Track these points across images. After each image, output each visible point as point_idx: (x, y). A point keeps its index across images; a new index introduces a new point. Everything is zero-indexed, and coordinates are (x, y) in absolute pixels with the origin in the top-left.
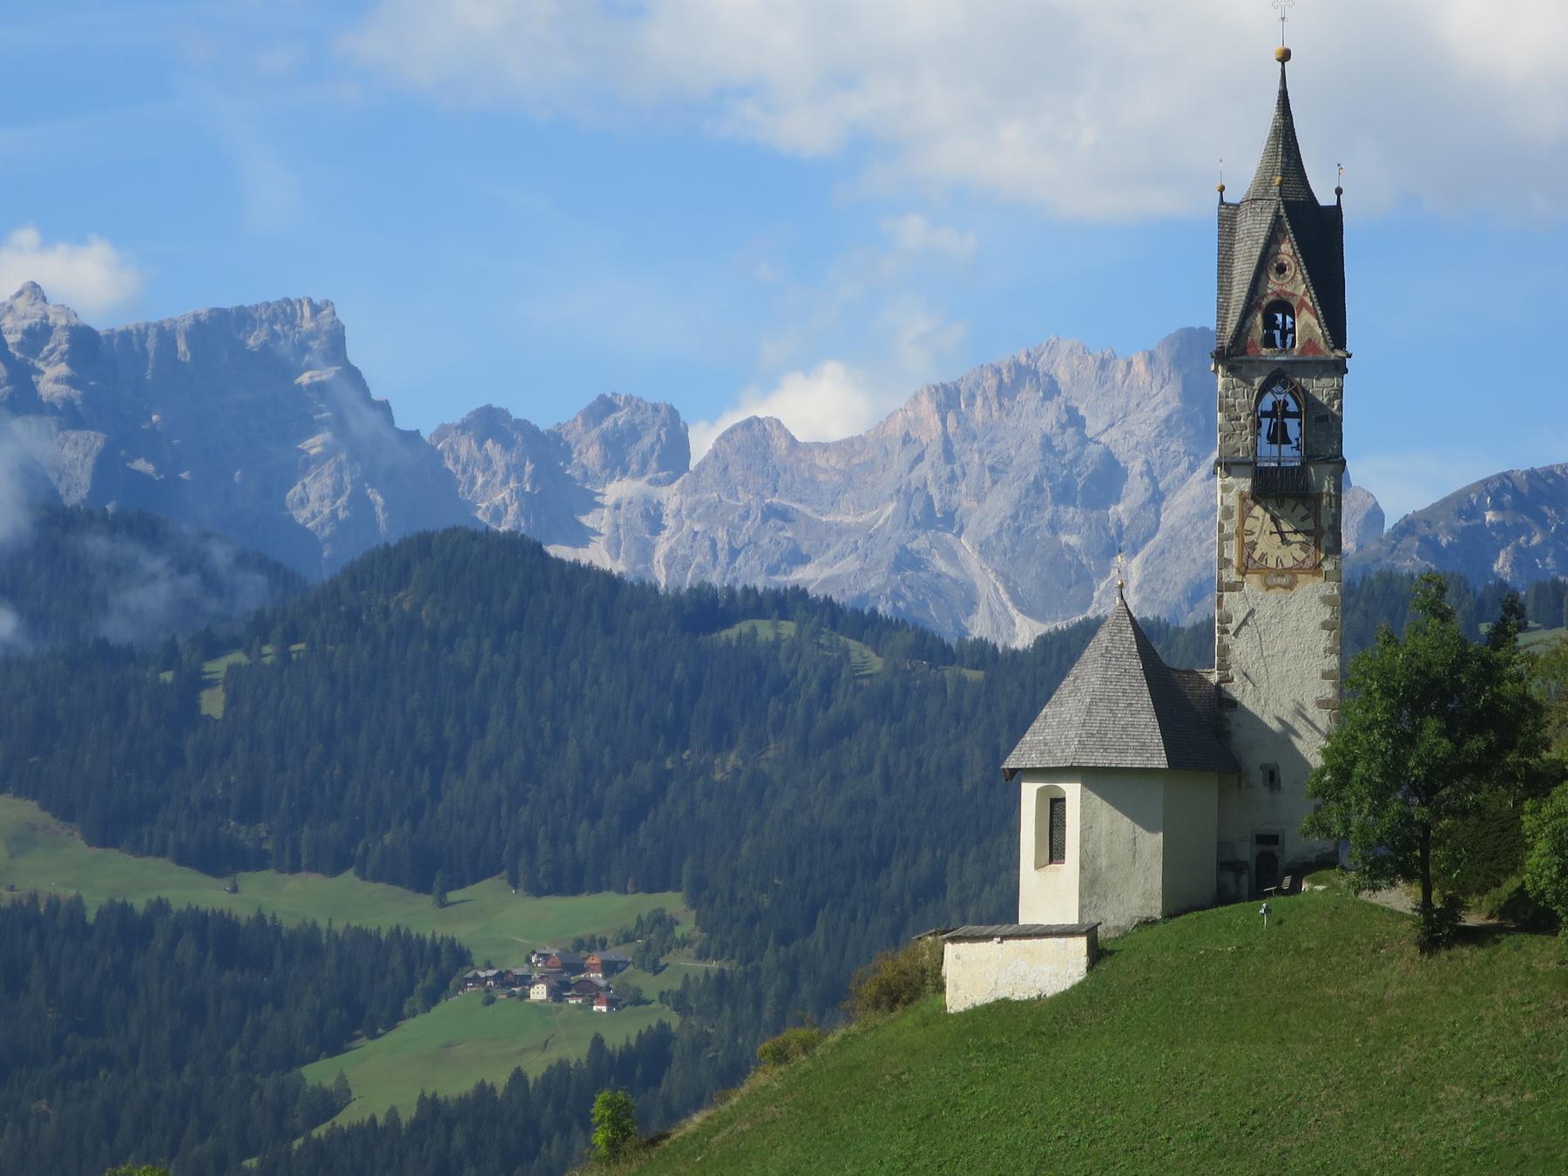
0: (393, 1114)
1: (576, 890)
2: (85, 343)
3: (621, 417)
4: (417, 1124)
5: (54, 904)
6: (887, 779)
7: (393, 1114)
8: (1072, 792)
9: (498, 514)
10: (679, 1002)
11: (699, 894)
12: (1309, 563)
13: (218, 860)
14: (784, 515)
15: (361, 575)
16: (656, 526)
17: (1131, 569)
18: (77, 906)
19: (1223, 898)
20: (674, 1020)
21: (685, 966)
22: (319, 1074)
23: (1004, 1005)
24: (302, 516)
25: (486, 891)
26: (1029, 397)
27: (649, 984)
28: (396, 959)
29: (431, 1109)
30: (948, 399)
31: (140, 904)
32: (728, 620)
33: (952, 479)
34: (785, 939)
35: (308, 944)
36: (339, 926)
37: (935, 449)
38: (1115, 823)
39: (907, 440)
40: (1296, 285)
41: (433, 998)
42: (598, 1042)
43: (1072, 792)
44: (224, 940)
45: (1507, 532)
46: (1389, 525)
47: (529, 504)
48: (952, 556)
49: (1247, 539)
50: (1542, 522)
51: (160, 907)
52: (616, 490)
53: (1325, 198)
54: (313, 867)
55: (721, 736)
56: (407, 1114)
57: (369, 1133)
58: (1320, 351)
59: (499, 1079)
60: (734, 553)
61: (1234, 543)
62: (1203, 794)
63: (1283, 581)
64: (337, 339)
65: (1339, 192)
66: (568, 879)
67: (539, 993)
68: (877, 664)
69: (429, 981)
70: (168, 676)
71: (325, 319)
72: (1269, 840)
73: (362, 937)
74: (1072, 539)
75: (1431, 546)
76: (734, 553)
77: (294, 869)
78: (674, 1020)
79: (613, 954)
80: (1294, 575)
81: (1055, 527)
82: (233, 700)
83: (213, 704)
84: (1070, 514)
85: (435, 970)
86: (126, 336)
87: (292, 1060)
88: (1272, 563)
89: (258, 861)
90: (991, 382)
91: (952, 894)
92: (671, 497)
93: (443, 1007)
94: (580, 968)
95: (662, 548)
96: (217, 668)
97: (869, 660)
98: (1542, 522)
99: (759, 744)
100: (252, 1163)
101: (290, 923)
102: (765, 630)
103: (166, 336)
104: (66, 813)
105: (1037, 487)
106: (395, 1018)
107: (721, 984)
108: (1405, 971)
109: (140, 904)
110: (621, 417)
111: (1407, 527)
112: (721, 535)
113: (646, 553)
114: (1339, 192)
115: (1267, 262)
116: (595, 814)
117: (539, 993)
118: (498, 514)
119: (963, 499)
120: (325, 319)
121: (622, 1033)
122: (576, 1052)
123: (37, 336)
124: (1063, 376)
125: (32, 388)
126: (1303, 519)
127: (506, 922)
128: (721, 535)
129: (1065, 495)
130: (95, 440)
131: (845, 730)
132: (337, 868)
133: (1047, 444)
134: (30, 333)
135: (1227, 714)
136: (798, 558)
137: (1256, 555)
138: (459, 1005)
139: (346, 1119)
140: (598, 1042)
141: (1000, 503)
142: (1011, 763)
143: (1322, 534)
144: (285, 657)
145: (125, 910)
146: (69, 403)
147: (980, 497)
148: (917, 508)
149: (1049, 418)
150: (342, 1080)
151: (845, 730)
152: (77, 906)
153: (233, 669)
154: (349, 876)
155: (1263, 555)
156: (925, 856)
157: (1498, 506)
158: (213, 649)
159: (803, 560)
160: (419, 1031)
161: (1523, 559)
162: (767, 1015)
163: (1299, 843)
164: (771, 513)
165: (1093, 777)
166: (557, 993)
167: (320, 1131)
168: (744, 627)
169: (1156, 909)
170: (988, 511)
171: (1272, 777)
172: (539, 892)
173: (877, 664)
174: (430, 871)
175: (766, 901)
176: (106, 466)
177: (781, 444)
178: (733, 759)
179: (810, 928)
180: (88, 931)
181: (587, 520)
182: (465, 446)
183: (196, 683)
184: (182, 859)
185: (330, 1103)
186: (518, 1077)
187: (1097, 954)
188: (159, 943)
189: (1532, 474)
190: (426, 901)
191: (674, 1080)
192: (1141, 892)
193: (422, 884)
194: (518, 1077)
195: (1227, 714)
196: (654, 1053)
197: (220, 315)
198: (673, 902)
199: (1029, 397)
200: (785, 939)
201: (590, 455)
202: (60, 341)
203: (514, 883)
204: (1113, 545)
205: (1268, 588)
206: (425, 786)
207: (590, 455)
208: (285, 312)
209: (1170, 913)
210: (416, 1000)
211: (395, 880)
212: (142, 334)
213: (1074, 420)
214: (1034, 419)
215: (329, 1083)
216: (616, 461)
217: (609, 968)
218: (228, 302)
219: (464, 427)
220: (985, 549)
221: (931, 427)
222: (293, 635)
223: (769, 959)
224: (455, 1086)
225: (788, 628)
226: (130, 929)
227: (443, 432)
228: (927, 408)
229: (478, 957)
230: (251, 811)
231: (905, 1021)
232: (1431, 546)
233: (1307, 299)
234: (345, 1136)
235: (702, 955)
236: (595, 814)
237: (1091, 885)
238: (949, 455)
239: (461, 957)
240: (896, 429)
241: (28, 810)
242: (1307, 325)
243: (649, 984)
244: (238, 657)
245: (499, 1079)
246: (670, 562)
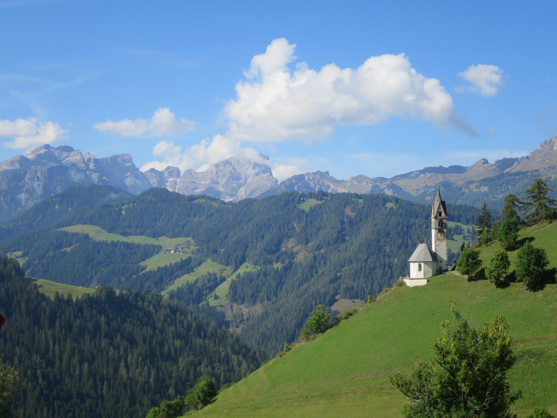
0: (154, 269)
1: (176, 237)
2: (96, 161)
3: (171, 169)
4: (157, 271)
5: (103, 241)
6: (219, 221)
7: (154, 269)
8: (422, 264)
9: (154, 183)
10: (192, 253)
11: (193, 238)
13: (125, 234)
14: (194, 182)
15: (143, 194)
16: (176, 184)
17: (242, 189)
18: (107, 241)
19: (437, 275)
20: (192, 255)
21: (193, 248)
22: (142, 264)
23: (417, 286)
24: (127, 184)
25: (163, 238)
26: (228, 165)
27: (188, 250)
28: (152, 248)
29: (159, 268)
30: (217, 166)
31: (115, 241)
32: (195, 199)
33: (218, 177)
34: (207, 243)
35: (139, 246)
36: (143, 243)
37: (215, 173)
38: (427, 267)
39: (211, 172)
40: (442, 210)
41: (157, 253)
42: (182, 259)
43: (422, 264)
44: (128, 246)
45: (296, 183)
46: (279, 183)
47: (158, 182)
48: (218, 188)
50: (301, 181)
51: (118, 241)
52: (171, 179)
54: (139, 235)
55: (195, 216)
56: (156, 269)
57: (151, 272)
59: (168, 264)
60: (187, 188)
62: (435, 263)
64: (131, 159)
66: (175, 236)
67: (172, 252)
68: (216, 205)
69: (157, 250)
70: (117, 209)
71: (129, 156)
72: (441, 268)
73: (147, 245)
74: (235, 185)
75: (286, 186)
76: (187, 188)
77: (136, 235)
78: (192, 255)
79: (182, 246)
81: (232, 184)
82: (126, 212)
83: (123, 213)
84: (234, 181)
85: (157, 249)
86: (101, 159)
87: (138, 262)
89: (131, 234)
90: (223, 163)
91: (229, 237)
92: (178, 180)
93: (159, 254)
94: (177, 248)
95: (177, 187)
96: (124, 207)
97: (215, 205)
98: (301, 181)
99: (200, 216)
100: (134, 276)
101: (136, 243)
102: (200, 201)
103: (107, 159)
104: (104, 228)
105: (229, 178)
106: (152, 256)
107: (198, 250)
108: (467, 284)
109: (115, 241)
110: (171, 169)
111: (282, 183)
112: (185, 186)
113: (175, 188)
115: (439, 208)
116: (178, 227)
117: (172, 252)
118: (154, 183)
119: (219, 180)
120: (129, 156)
121: (185, 257)
122: (179, 260)
123: (89, 160)
124: (233, 162)
125: (89, 167)
127: (165, 242)
128: (185, 186)
129: (233, 179)
130: (98, 174)
131: (212, 214)
132: (142, 235)
133: (231, 172)
134: (88, 159)
136: (196, 188)
138: (161, 254)
139: (147, 270)
140: (182, 259)
141: (224, 180)
142: (410, 260)
144: (133, 206)
145: (113, 242)
146: (94, 169)
147: (222, 179)
148: (213, 181)
149: (231, 168)
150: (146, 265)
151: (212, 214)
152: (107, 241)
153: (126, 208)
154: (144, 236)
156: (225, 232)
157: (295, 180)
158: (123, 205)
159: (197, 189)
160: (155, 257)
161: (298, 187)
162: (205, 254)
163: (444, 268)
164: (192, 182)
165: (424, 262)
166: (175, 252)
167: (144, 272)
168: (198, 200)
169: (431, 276)
170: (223, 181)
171: (441, 261)
172: (171, 238)
173: (216, 205)
174: (155, 235)
175: (203, 238)
176: (100, 178)
177: (193, 173)
178: (197, 219)
179: (210, 242)
180: (108, 245)
181: (167, 184)
182: (149, 174)
183: (121, 210)
184: (120, 234)
185: (144, 268)
186: (171, 264)
187: (428, 281)
188: (118, 246)
189: (299, 175)
190: (155, 239)
191: (192, 264)
192: (430, 274)
193: (154, 237)
194: (171, 264)
196: (190, 259)
197: (114, 156)
198: (190, 239)
199: (228, 165)
200: (207, 243)
201: (167, 175)
202: (92, 161)
203: (167, 236)
204: (240, 186)
206: (154, 223)
207: (167, 175)
208: (123, 155)
209: (433, 276)
210: (155, 253)
211: (150, 236)
212: (103, 159)
213: (235, 168)
214: (229, 168)
215: (144, 265)
216: (170, 175)
217: (182, 248)
218: (115, 154)
219: (149, 171)
220: (222, 187)
221: (214, 170)
222: (134, 203)
223: (205, 246)
224: (162, 265)
225: (204, 200)
226: (114, 244)
227: (146, 171)
228: (214, 167)
229: (163, 247)
230: (130, 227)
231: (402, 288)
232: (286, 186)
234: (147, 273)
235: (195, 246)
236: (178, 227)
237: (425, 273)
238: (217, 174)
239: (161, 247)
240: (209, 170)
241: (98, 228)
243: (188, 250)
244: (126, 206)
245: (168, 264)
246: (178, 189)
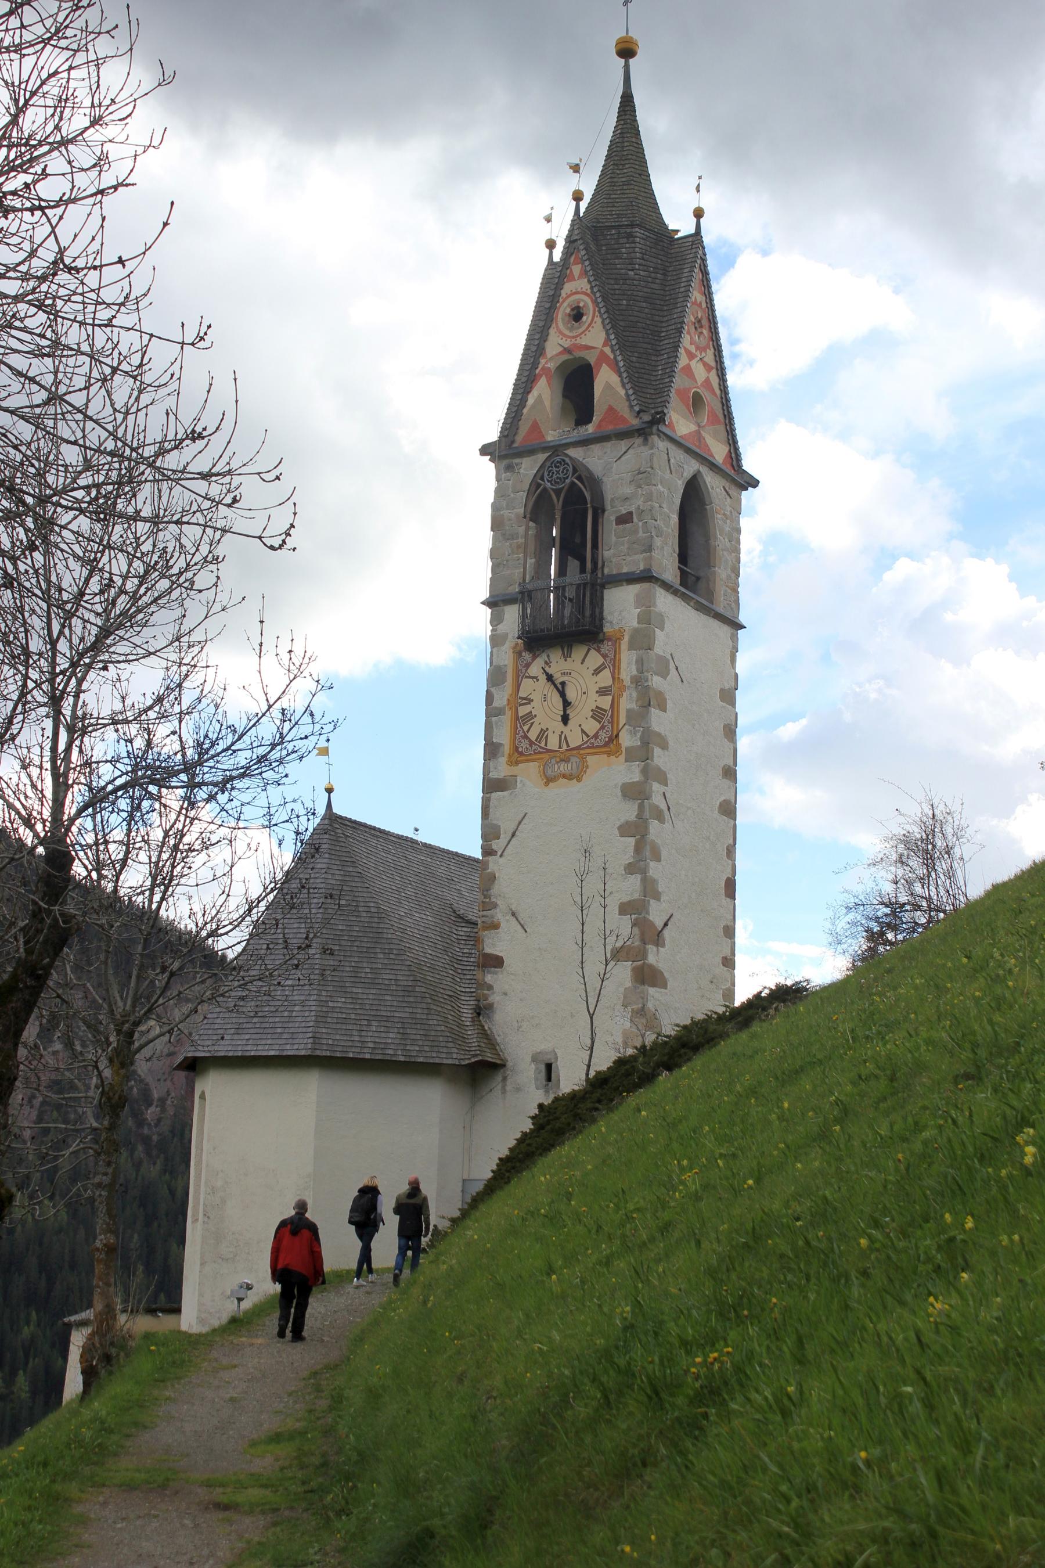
12: (604, 736)
36: (540, 1162)
49: (523, 711)
53: (678, 221)
58: (623, 420)
61: (507, 719)
63: (564, 768)
65: (699, 214)
80: (583, 758)
88: (553, 743)
114: (699, 214)
126: (597, 672)
135: (489, 978)
137: (533, 735)
143: (622, 689)
155: (543, 732)
195: (489, 978)
205: (549, 780)
233: (607, 350)
242: (608, 386)
